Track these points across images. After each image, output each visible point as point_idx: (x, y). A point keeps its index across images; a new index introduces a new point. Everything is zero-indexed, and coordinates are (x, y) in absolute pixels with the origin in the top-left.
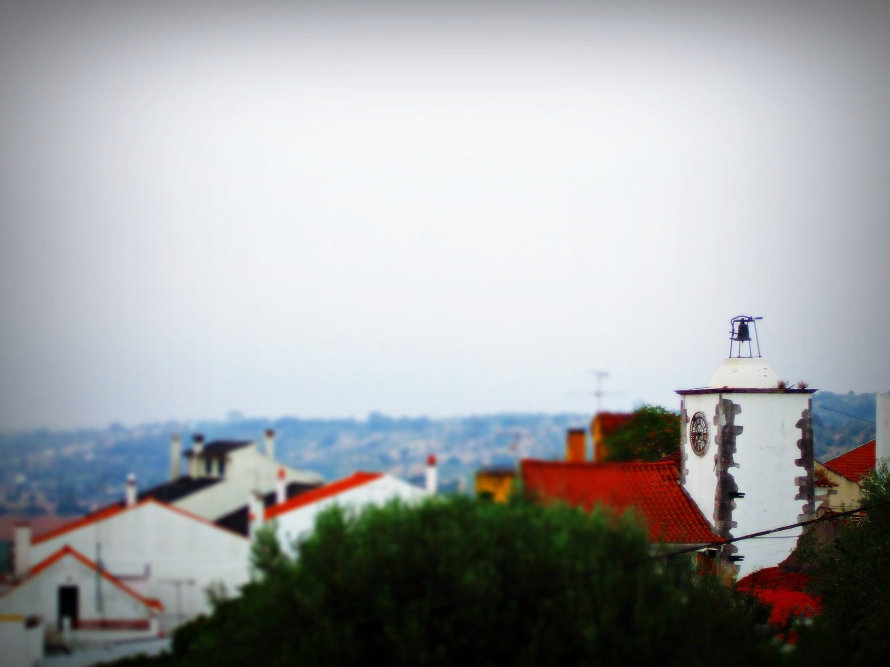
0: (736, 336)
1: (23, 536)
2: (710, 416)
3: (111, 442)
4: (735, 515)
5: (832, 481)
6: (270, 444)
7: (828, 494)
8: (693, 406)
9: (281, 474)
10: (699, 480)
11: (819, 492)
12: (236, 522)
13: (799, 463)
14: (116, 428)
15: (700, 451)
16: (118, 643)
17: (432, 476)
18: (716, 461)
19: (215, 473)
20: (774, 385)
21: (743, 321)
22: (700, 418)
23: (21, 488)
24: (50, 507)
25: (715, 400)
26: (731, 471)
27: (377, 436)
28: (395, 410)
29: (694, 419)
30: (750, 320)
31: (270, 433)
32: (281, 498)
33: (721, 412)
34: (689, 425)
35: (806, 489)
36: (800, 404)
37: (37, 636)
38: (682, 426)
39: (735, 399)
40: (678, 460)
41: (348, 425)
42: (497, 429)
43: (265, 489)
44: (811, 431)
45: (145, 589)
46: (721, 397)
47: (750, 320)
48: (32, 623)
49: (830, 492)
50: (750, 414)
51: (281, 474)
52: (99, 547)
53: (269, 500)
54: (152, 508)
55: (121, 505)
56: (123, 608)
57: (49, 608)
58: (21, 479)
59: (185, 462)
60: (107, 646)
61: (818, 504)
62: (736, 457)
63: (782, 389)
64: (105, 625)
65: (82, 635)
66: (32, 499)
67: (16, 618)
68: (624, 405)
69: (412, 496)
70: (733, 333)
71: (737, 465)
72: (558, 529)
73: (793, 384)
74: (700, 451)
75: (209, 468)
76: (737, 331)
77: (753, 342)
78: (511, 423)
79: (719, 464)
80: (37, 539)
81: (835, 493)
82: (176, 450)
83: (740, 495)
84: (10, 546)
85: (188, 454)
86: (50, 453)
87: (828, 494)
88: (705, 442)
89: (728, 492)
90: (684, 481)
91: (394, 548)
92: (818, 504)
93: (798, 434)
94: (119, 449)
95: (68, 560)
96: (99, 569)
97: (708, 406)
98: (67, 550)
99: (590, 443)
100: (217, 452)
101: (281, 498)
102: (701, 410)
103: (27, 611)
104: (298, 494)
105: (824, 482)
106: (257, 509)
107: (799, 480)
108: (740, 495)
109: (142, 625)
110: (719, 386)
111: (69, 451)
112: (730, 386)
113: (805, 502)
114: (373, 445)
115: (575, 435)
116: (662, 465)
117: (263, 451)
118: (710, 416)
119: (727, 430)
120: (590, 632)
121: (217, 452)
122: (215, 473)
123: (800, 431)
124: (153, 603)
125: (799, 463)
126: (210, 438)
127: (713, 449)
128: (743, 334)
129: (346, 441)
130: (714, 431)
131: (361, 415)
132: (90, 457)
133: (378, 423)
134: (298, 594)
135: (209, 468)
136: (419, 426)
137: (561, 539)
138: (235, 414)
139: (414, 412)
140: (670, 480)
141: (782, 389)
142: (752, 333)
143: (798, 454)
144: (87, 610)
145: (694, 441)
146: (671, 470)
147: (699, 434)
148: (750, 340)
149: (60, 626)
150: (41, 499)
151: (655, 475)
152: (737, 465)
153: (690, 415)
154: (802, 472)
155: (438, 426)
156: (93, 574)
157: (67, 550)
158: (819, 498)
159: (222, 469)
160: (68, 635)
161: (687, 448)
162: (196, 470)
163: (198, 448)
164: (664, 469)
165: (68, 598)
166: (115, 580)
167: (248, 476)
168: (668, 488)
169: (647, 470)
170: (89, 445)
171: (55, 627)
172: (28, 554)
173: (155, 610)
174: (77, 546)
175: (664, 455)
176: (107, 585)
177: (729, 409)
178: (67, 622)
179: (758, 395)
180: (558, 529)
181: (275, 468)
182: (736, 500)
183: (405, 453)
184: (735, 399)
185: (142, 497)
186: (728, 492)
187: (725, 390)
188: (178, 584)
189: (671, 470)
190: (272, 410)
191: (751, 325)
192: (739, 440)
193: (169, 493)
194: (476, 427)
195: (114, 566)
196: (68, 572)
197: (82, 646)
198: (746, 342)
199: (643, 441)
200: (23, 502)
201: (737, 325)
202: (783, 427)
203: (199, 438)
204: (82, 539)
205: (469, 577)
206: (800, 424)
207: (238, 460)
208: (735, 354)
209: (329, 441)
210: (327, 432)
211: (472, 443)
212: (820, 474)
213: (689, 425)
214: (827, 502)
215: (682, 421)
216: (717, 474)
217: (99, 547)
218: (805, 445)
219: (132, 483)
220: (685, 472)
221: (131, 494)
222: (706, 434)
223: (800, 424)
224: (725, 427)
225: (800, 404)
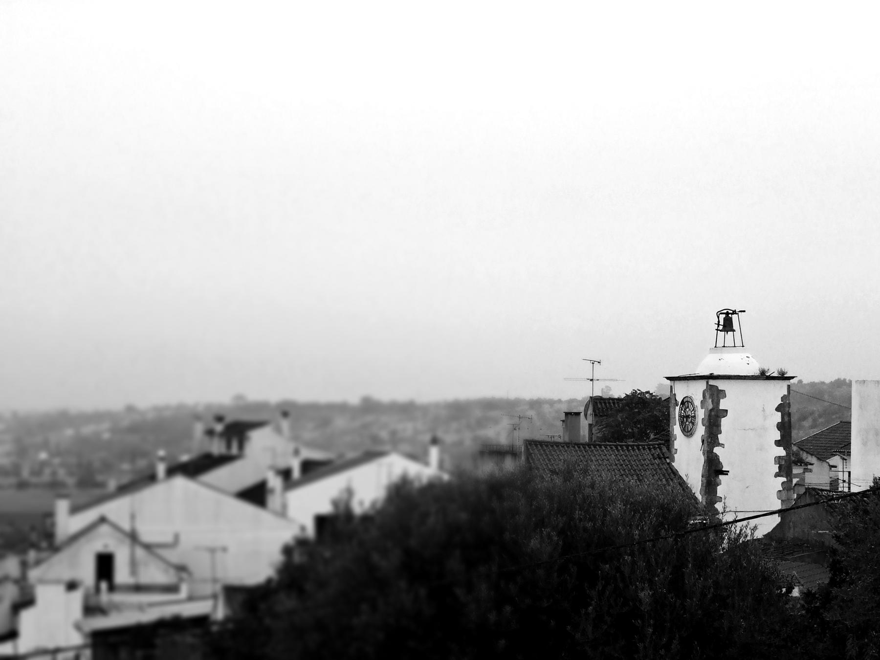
0: (721, 328)
1: (62, 507)
2: (697, 400)
3: (126, 423)
4: (720, 491)
5: (807, 460)
6: (285, 424)
7: (804, 472)
8: (681, 391)
9: (296, 452)
10: (687, 457)
11: (796, 470)
12: (256, 494)
13: (778, 443)
14: (130, 409)
15: (688, 432)
16: (152, 605)
17: (434, 453)
18: (703, 441)
19: (234, 450)
20: (756, 372)
21: (727, 314)
22: (688, 402)
23: (43, 464)
24: (71, 481)
25: (702, 386)
26: (717, 450)
27: (369, 418)
28: (385, 394)
29: (683, 403)
30: (734, 312)
31: (285, 414)
32: (296, 474)
33: (707, 396)
34: (677, 408)
35: (785, 467)
36: (779, 390)
37: (76, 599)
38: (671, 409)
39: (721, 385)
40: (667, 440)
41: (342, 408)
42: (478, 413)
43: (282, 464)
44: (789, 415)
45: (174, 556)
46: (707, 383)
47: (734, 312)
48: (72, 586)
49: (806, 470)
50: (733, 399)
51: (296, 452)
52: (133, 517)
53: (286, 474)
54: (180, 482)
55: (151, 478)
56: (154, 574)
57: (87, 573)
58: (43, 456)
59: (206, 439)
60: (141, 608)
61: (795, 481)
62: (721, 438)
63: (763, 376)
64: (138, 588)
65: (118, 598)
66: (54, 474)
67: (57, 582)
68: (620, 391)
69: (426, 471)
70: (719, 325)
71: (722, 445)
72: (612, 500)
73: (773, 372)
74: (688, 432)
75: (229, 446)
76: (722, 323)
77: (737, 333)
78: (491, 406)
79: (706, 445)
80: (75, 510)
81: (811, 471)
82: (199, 429)
83: (726, 473)
84: (50, 515)
85: (210, 433)
86: (69, 432)
87: (804, 472)
88: (693, 424)
89: (714, 470)
90: (673, 460)
91: (463, 516)
92: (795, 481)
93: (778, 417)
94: (134, 429)
95: (104, 529)
96: (133, 537)
97: (696, 391)
98: (103, 520)
99: (584, 423)
100: (237, 431)
101: (296, 474)
102: (690, 395)
103: (68, 575)
104: (312, 470)
105: (800, 462)
106: (275, 482)
107: (778, 459)
108: (726, 473)
109: (172, 589)
110: (706, 373)
111: (88, 430)
112: (716, 373)
113: (784, 479)
114: (365, 426)
115: (571, 416)
116: (621, 446)
117: (278, 430)
118: (697, 400)
119: (713, 413)
120: (645, 595)
121: (237, 431)
122: (234, 450)
123: (779, 415)
124: (181, 569)
125: (778, 443)
126: (230, 418)
127: (700, 430)
128: (727, 326)
129: (340, 423)
130: (701, 414)
131: (354, 399)
132: (106, 436)
133: (369, 406)
134: (376, 558)
135: (229, 446)
136: (407, 409)
137: (616, 509)
138: (239, 397)
139: (401, 395)
140: (660, 458)
141: (763, 376)
142: (736, 325)
143: (777, 435)
144: (122, 575)
145: (682, 423)
146: (661, 449)
147: (688, 417)
148: (734, 331)
149: (98, 590)
150: (62, 474)
151: (647, 455)
152: (722, 445)
153: (679, 400)
154: (781, 452)
155: (424, 409)
156: (128, 541)
157: (103, 520)
158: (796, 476)
159: (241, 446)
160: (105, 597)
161: (677, 429)
162: (217, 447)
163: (219, 428)
164: (655, 448)
165: (105, 565)
166: (148, 547)
167: (264, 454)
168: (658, 465)
169: (639, 449)
170: (105, 426)
171: (92, 590)
172: (67, 523)
173: (184, 575)
174: (112, 517)
175: (652, 436)
176: (140, 552)
177: (715, 394)
178: (104, 585)
179: (732, 381)
180: (612, 500)
181: (291, 447)
182: (721, 477)
183: (393, 433)
184: (721, 385)
185: (174, 470)
186: (714, 470)
187: (712, 377)
188: (212, 551)
189: (661, 449)
190: (274, 395)
191: (734, 317)
192: (724, 422)
193: (198, 467)
194: (458, 411)
195: (148, 534)
196: (103, 541)
197: (118, 608)
198: (730, 333)
199: (636, 422)
200: (46, 477)
201: (722, 317)
202: (764, 410)
203: (219, 419)
204: (117, 509)
205: (534, 543)
206: (778, 409)
207: (258, 439)
208: (720, 344)
209: (325, 422)
210: (320, 415)
211: (454, 425)
212: (796, 454)
213: (677, 408)
214: (803, 479)
215: (672, 405)
216: (704, 454)
217: (133, 517)
218: (784, 427)
219: (162, 459)
220: (674, 451)
221: (161, 469)
222: (694, 417)
223: (778, 409)
224: (711, 410)
225: (779, 390)
